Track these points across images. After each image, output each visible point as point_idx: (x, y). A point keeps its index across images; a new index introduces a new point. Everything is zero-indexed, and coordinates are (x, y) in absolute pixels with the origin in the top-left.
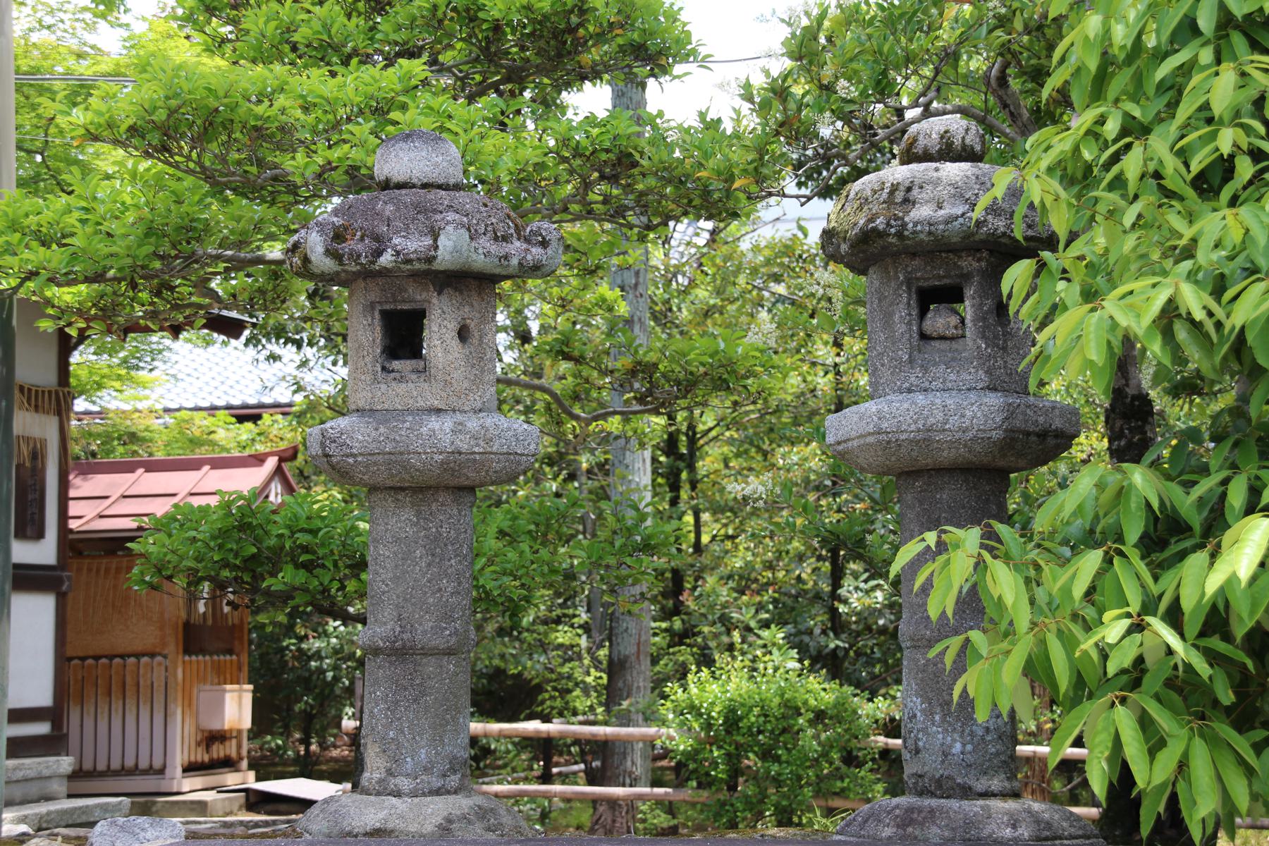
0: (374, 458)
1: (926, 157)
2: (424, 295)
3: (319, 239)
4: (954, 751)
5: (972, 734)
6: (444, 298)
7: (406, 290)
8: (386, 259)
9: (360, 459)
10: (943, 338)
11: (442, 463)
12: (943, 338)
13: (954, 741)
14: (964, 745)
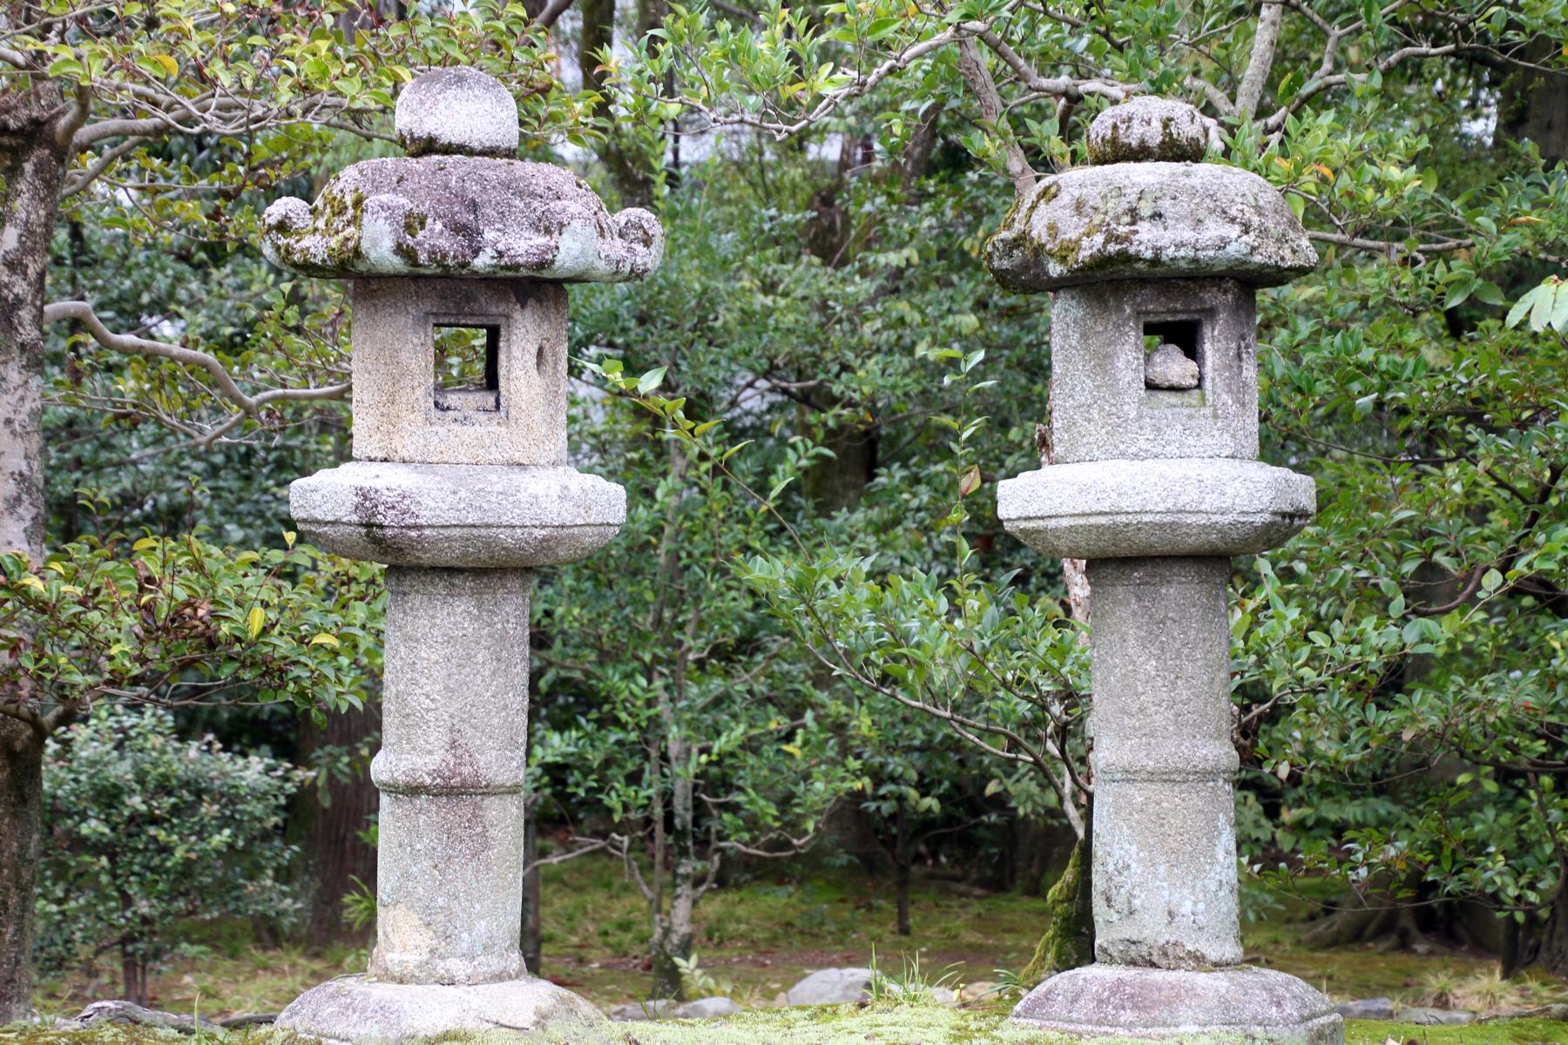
0: (447, 532)
1: (1140, 153)
2: (502, 308)
3: (387, 228)
4: (1183, 910)
5: (1205, 890)
6: (528, 311)
7: (476, 300)
8: (483, 261)
9: (427, 532)
10: (1173, 389)
11: (544, 539)
12: (1173, 389)
13: (1183, 898)
14: (1195, 903)
